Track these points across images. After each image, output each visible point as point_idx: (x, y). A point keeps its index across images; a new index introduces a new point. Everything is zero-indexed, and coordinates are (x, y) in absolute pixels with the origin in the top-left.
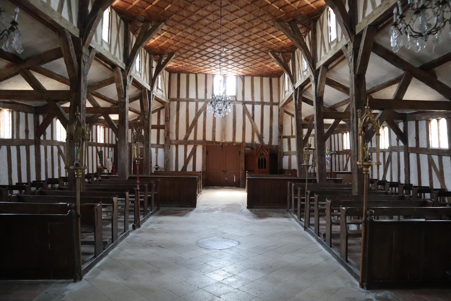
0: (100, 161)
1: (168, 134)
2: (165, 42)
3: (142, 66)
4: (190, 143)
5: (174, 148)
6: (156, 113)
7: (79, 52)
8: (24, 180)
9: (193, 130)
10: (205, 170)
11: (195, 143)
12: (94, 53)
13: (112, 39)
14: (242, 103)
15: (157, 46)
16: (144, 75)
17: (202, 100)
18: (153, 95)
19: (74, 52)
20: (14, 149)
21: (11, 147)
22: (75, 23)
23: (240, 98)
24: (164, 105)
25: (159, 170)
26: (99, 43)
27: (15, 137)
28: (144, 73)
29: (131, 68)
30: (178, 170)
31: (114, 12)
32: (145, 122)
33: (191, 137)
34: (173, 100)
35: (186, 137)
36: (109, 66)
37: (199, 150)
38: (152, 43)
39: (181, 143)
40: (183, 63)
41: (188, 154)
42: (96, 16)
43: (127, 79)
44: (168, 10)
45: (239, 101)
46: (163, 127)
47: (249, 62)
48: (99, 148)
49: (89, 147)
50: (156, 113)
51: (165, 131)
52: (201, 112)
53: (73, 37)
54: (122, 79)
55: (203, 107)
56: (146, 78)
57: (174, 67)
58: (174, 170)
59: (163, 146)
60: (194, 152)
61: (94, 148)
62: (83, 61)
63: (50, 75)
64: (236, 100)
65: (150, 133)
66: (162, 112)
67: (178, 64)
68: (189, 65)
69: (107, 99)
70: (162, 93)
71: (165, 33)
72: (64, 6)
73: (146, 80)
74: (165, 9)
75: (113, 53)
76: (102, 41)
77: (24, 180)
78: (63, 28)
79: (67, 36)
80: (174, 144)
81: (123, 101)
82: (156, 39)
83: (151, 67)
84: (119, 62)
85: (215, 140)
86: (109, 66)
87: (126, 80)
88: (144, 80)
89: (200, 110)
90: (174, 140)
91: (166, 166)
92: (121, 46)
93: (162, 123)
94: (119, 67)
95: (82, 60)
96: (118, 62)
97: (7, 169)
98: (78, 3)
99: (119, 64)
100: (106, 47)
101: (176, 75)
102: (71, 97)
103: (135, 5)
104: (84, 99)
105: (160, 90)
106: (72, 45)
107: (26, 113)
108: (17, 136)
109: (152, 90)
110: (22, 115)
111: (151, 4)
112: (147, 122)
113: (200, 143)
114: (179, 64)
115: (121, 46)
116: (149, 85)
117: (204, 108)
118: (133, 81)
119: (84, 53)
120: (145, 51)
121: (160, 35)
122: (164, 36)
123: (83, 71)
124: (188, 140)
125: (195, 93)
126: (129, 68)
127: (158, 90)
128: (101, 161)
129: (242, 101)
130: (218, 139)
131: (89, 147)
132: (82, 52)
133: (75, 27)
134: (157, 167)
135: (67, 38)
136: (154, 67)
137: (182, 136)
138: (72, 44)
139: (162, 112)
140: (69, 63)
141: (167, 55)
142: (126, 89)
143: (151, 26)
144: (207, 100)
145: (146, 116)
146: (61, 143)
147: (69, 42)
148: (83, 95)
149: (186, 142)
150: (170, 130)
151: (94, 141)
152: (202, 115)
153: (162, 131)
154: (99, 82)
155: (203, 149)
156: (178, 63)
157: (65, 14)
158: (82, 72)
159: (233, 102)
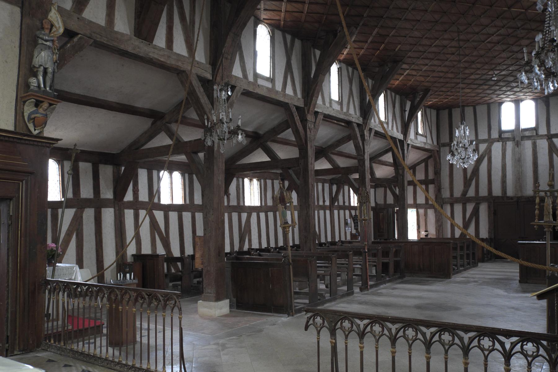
0: (355, 226)
1: (439, 190)
2: (412, 80)
3: (389, 114)
4: (470, 200)
5: (448, 208)
6: (423, 164)
7: (304, 121)
8: (273, 245)
9: (474, 183)
10: (493, 237)
11: (478, 200)
12: (321, 117)
13: (343, 96)
14: (547, 138)
15: (406, 87)
16: (393, 124)
17: (484, 141)
18: (408, 145)
19: (300, 121)
20: (262, 215)
21: (260, 213)
22: (299, 95)
23: (543, 131)
24: (431, 153)
25: (429, 237)
26: (327, 104)
27: (263, 204)
28: (393, 121)
29: (368, 121)
30: (454, 236)
31: (344, 66)
32: (399, 178)
33: (471, 193)
34: (444, 145)
35: (465, 193)
36: (343, 124)
37: (483, 209)
38: (398, 85)
39: (457, 201)
40: (447, 97)
41: (468, 215)
42: (317, 83)
43: (365, 133)
44: (399, 50)
45: (542, 136)
46: (432, 182)
47: (509, 90)
48: (353, 212)
49: (340, 211)
50: (423, 164)
51: (435, 187)
52: (484, 157)
53: (298, 108)
54: (358, 135)
55: (485, 151)
56: (397, 126)
57: (444, 101)
58: (449, 236)
59: (200, 208)
60: (476, 212)
61: (347, 212)
62: (309, 128)
63: (286, 143)
64: (537, 134)
65: (405, 191)
66: (431, 163)
67: (441, 99)
68: (456, 98)
69: (352, 156)
70: (425, 138)
71: (407, 71)
72: (288, 83)
73: (397, 129)
74: (396, 50)
75: (345, 110)
76: (331, 100)
77: (273, 245)
78: (287, 103)
79: (292, 109)
80: (447, 203)
81: (362, 158)
82: (400, 79)
83: (403, 111)
84: (353, 117)
85: (506, 194)
86: (343, 124)
87: (364, 135)
88: (392, 129)
89: (482, 155)
90: (448, 198)
91: (438, 232)
92: (356, 99)
93: (431, 176)
94: (354, 122)
95: (308, 127)
96: (351, 118)
97: (257, 234)
98: (301, 74)
99: (353, 120)
100: (337, 107)
101: (446, 112)
102: (301, 164)
103: (363, 55)
104: (311, 164)
105: (422, 135)
106: (297, 116)
107: (273, 180)
108: (265, 203)
109: (406, 138)
110: (269, 182)
111: (379, 49)
112: (401, 177)
113: (484, 199)
114: (443, 100)
115: (356, 99)
116: (402, 133)
117: (488, 151)
118: (375, 133)
119: (310, 120)
120: (393, 94)
121: (403, 74)
122: (408, 75)
123: (309, 137)
124: (467, 196)
125: (486, 130)
126: (366, 121)
127: (419, 137)
128: (356, 227)
129: (546, 135)
130: (510, 192)
131: (340, 211)
132: (307, 120)
133: (299, 99)
134: (427, 233)
135: (292, 111)
136: (406, 111)
137: (458, 193)
138: (297, 114)
139: (431, 163)
140: (296, 132)
141: (421, 93)
142: (365, 145)
143: (389, 68)
144: (492, 139)
145: (400, 171)
146: (412, 206)
147: (294, 114)
148: (310, 160)
149: (464, 200)
150: (442, 184)
151: (347, 204)
152: (486, 160)
153: (431, 187)
154: (337, 141)
155: (489, 207)
156: (445, 95)
157: (289, 91)
158: (308, 139)
159: (533, 138)
